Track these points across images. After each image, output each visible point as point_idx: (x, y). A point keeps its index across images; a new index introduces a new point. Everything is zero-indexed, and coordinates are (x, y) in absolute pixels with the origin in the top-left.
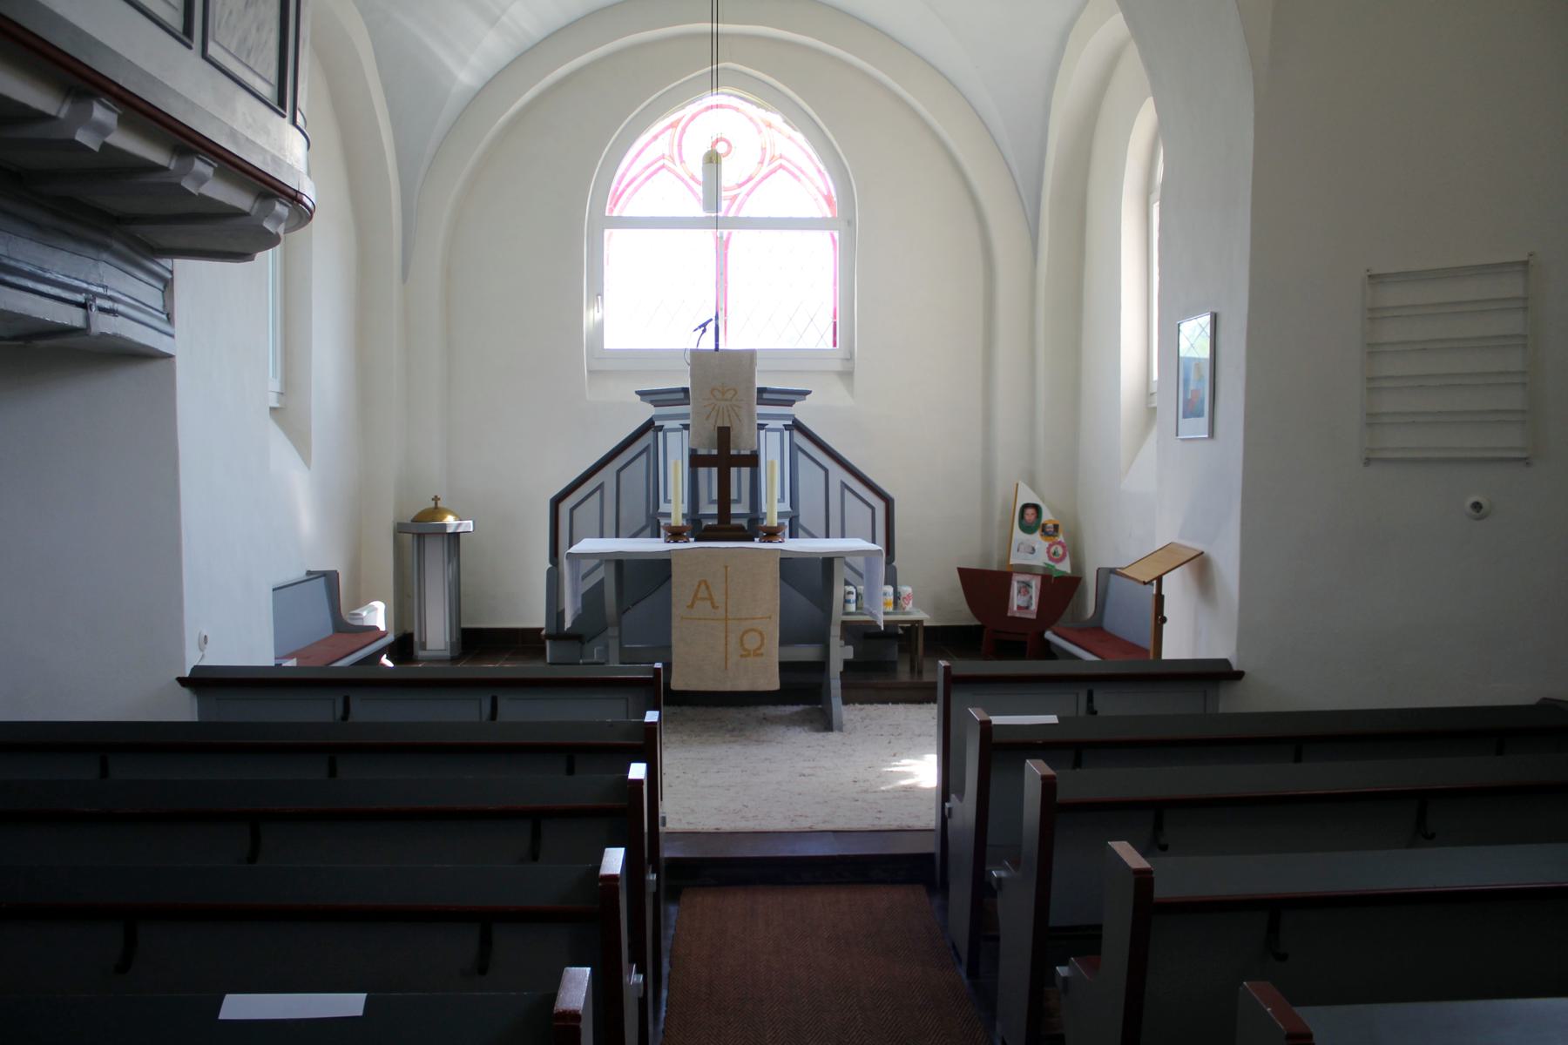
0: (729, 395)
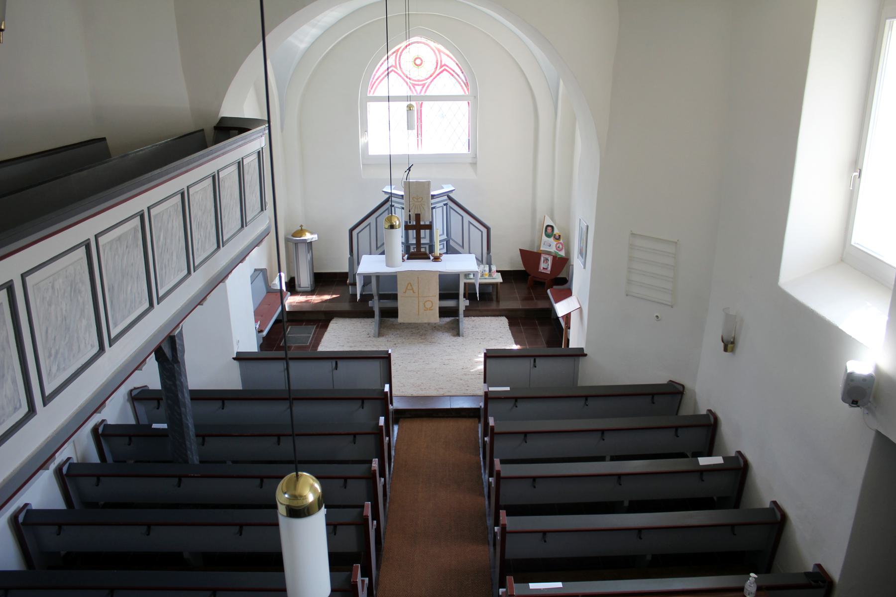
0: (420, 200)
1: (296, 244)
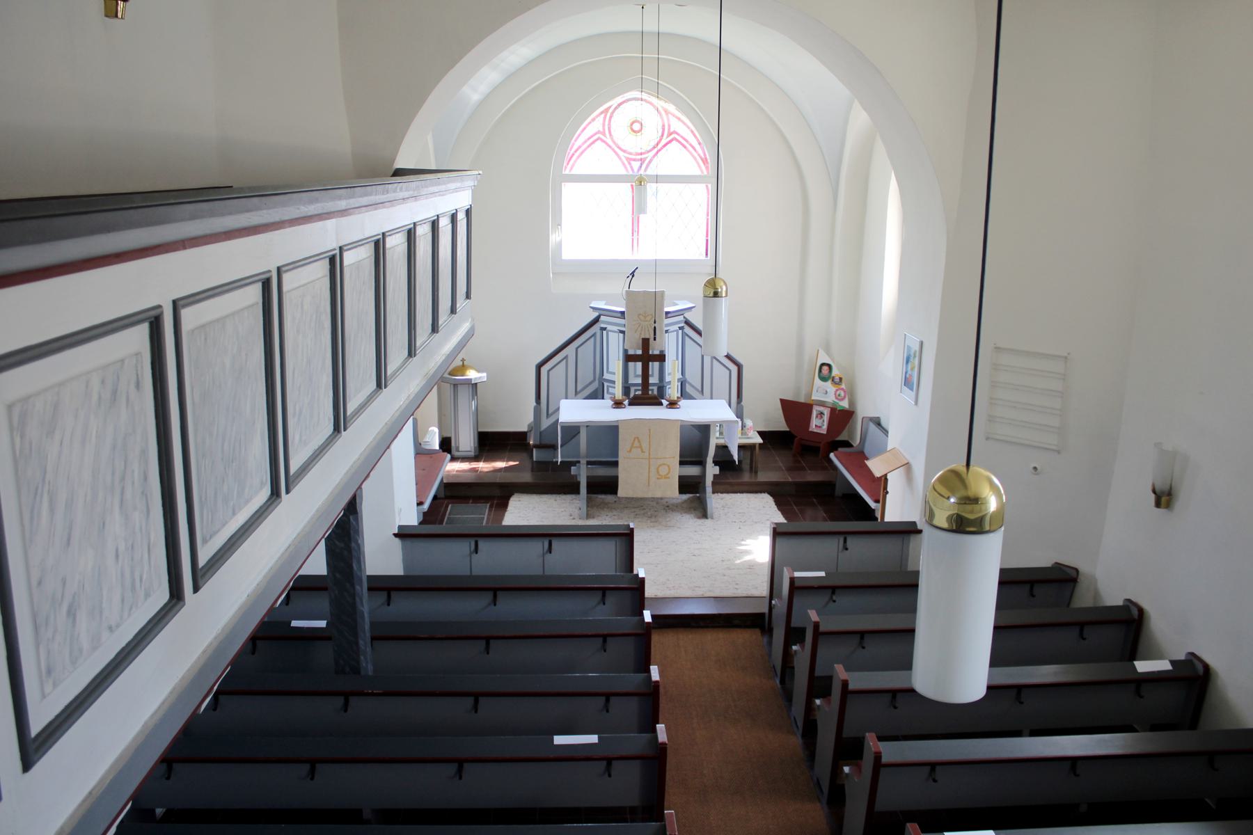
1: (455, 385)
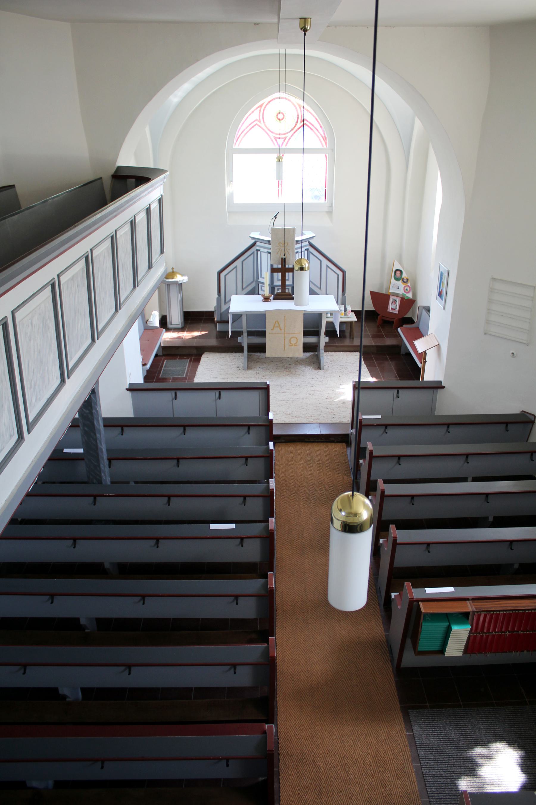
1: (169, 285)
